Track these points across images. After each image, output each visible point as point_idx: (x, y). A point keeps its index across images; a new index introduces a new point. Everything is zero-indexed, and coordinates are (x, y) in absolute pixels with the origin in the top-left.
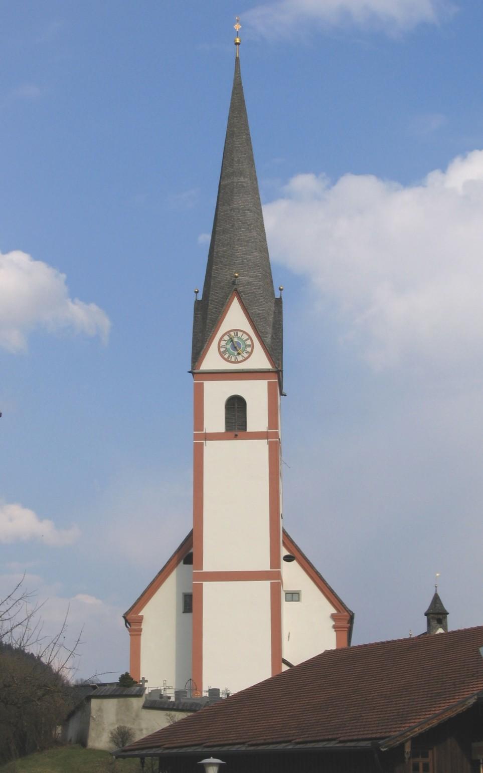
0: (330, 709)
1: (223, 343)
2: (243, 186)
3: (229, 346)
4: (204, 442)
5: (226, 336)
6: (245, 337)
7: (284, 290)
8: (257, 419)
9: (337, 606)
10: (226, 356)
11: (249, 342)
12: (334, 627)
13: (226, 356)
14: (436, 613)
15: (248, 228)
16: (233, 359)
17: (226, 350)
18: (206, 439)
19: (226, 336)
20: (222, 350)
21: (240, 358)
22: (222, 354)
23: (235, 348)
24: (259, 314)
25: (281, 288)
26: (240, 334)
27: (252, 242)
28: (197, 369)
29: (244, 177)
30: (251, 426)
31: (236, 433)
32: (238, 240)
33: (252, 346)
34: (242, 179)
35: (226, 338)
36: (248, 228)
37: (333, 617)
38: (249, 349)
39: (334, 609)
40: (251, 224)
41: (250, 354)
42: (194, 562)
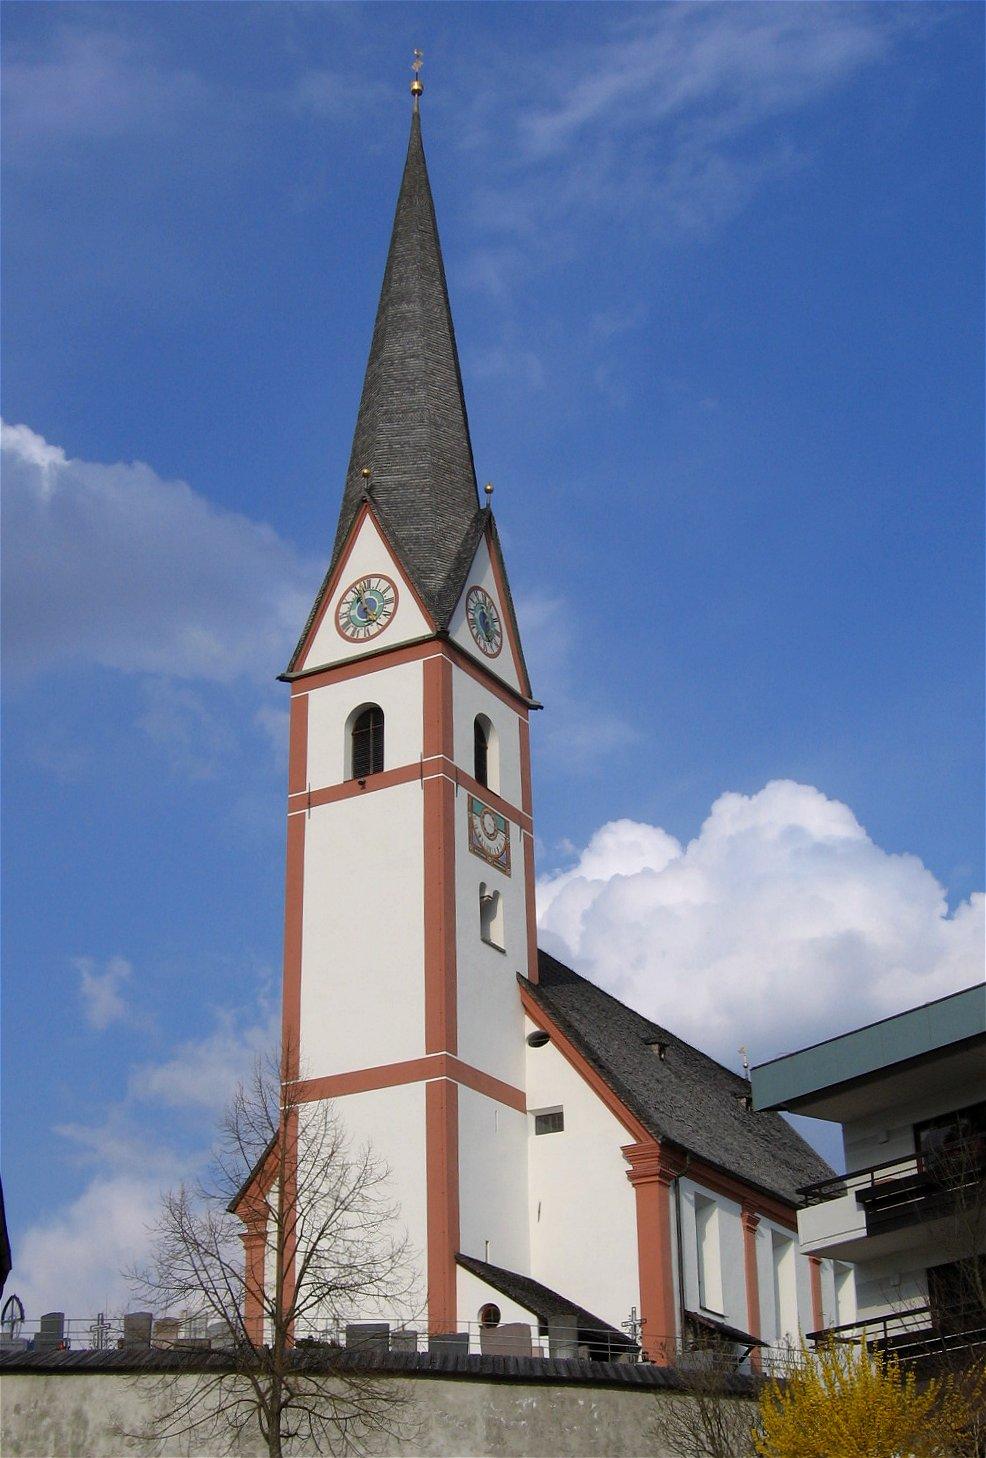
0: (270, 1276)
1: (344, 608)
2: (404, 318)
3: (354, 612)
4: (307, 811)
5: (351, 593)
6: (384, 584)
7: (495, 491)
8: (403, 743)
9: (636, 1131)
10: (348, 633)
11: (390, 594)
12: (631, 1176)
13: (348, 633)
14: (538, 1040)
15: (408, 388)
16: (361, 636)
17: (351, 620)
18: (309, 806)
19: (351, 593)
20: (342, 622)
21: (373, 629)
22: (341, 631)
23: (364, 612)
24: (417, 537)
25: (489, 487)
26: (374, 582)
27: (414, 411)
28: (297, 670)
29: (408, 303)
30: (393, 760)
31: (362, 779)
32: (385, 413)
33: (396, 600)
34: (405, 307)
35: (351, 596)
36: (408, 388)
37: (627, 1151)
38: (390, 608)
39: (630, 1137)
40: (417, 379)
41: (392, 615)
42: (565, 1128)
